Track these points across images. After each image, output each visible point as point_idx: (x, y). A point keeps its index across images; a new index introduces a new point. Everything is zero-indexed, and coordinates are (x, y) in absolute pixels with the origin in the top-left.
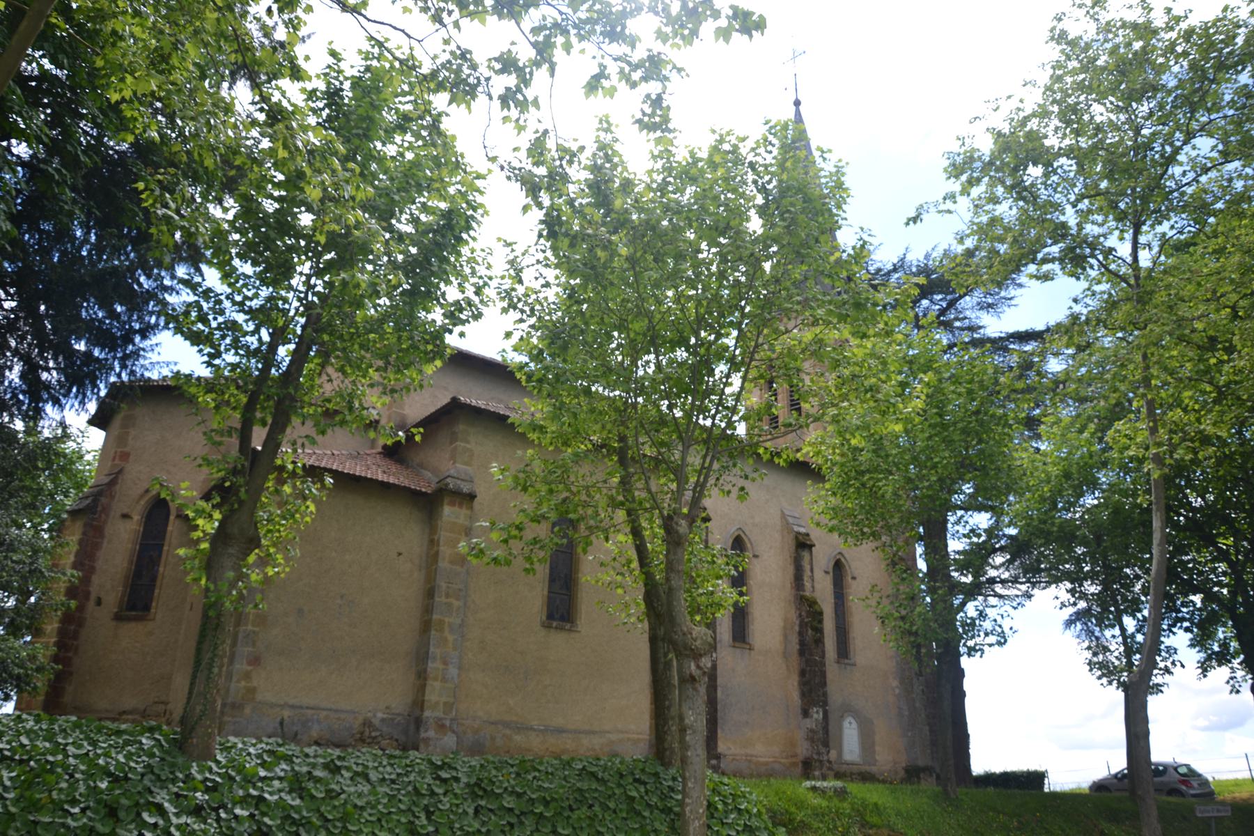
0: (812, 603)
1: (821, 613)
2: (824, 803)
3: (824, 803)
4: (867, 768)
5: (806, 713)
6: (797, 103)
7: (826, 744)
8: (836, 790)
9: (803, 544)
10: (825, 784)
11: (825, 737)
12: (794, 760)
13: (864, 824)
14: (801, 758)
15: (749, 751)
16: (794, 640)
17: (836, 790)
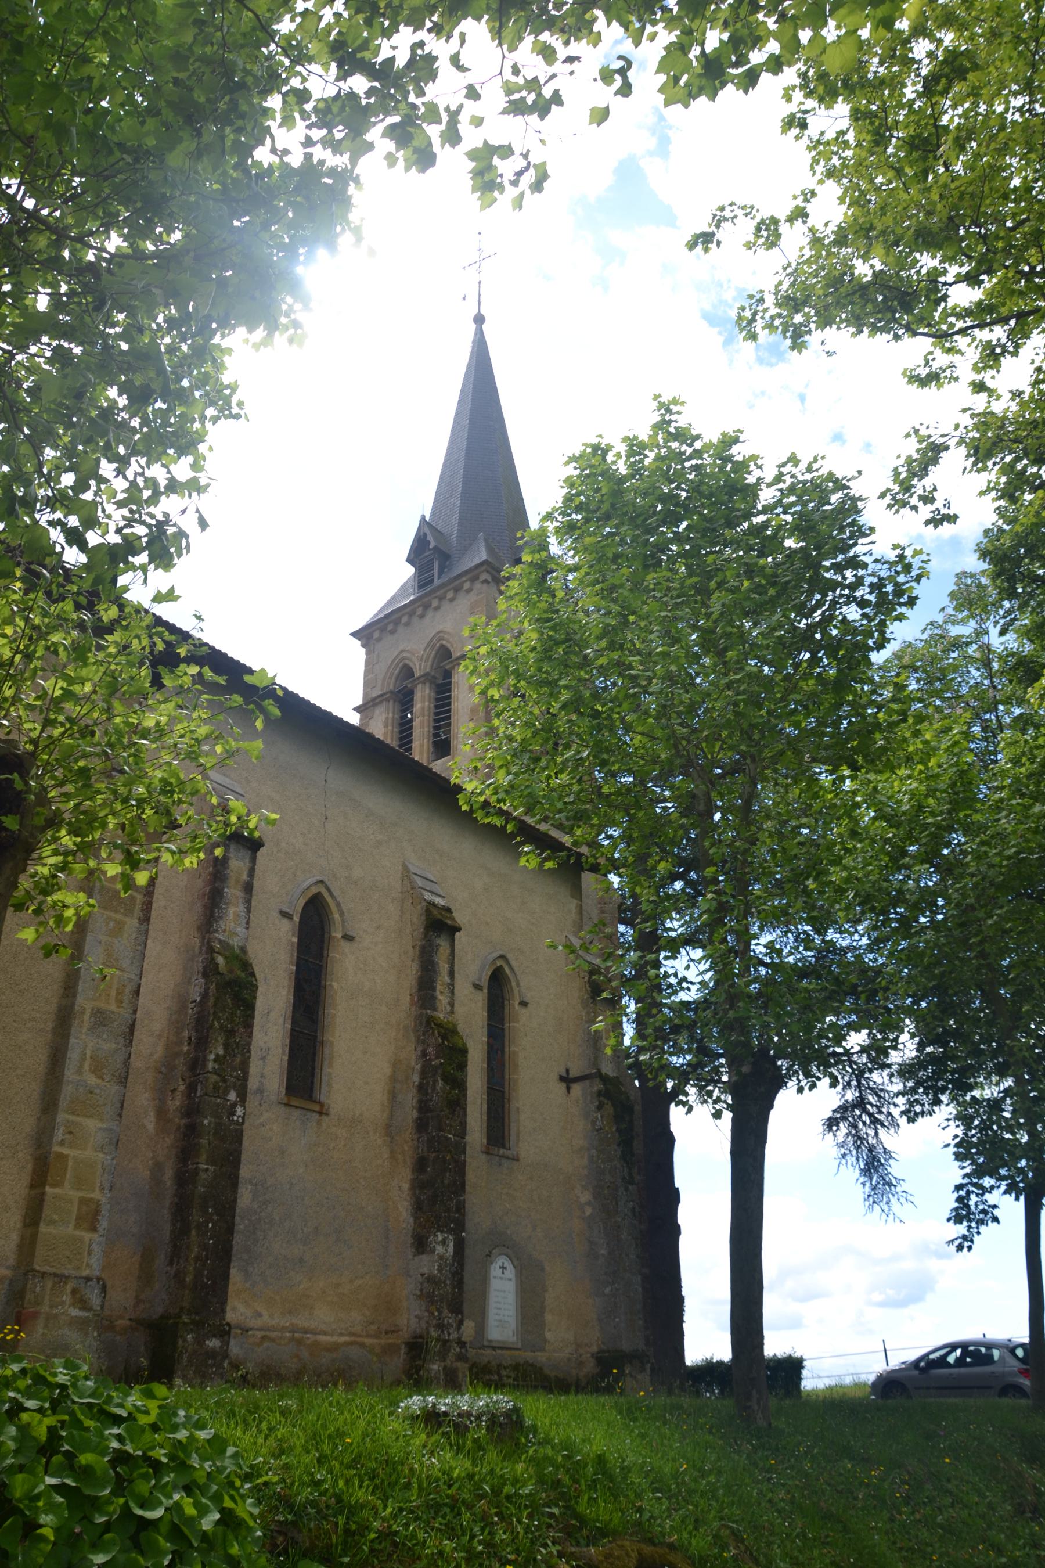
0: (448, 1032)
1: (464, 1052)
2: (460, 1467)
3: (460, 1467)
4: (528, 1355)
5: (421, 1245)
6: (479, 319)
7: (457, 1308)
8: (493, 1420)
9: (439, 925)
10: (464, 1401)
11: (454, 1294)
12: (392, 1339)
13: (575, 1528)
14: (405, 1335)
15: (301, 1322)
16: (409, 1100)
17: (493, 1420)
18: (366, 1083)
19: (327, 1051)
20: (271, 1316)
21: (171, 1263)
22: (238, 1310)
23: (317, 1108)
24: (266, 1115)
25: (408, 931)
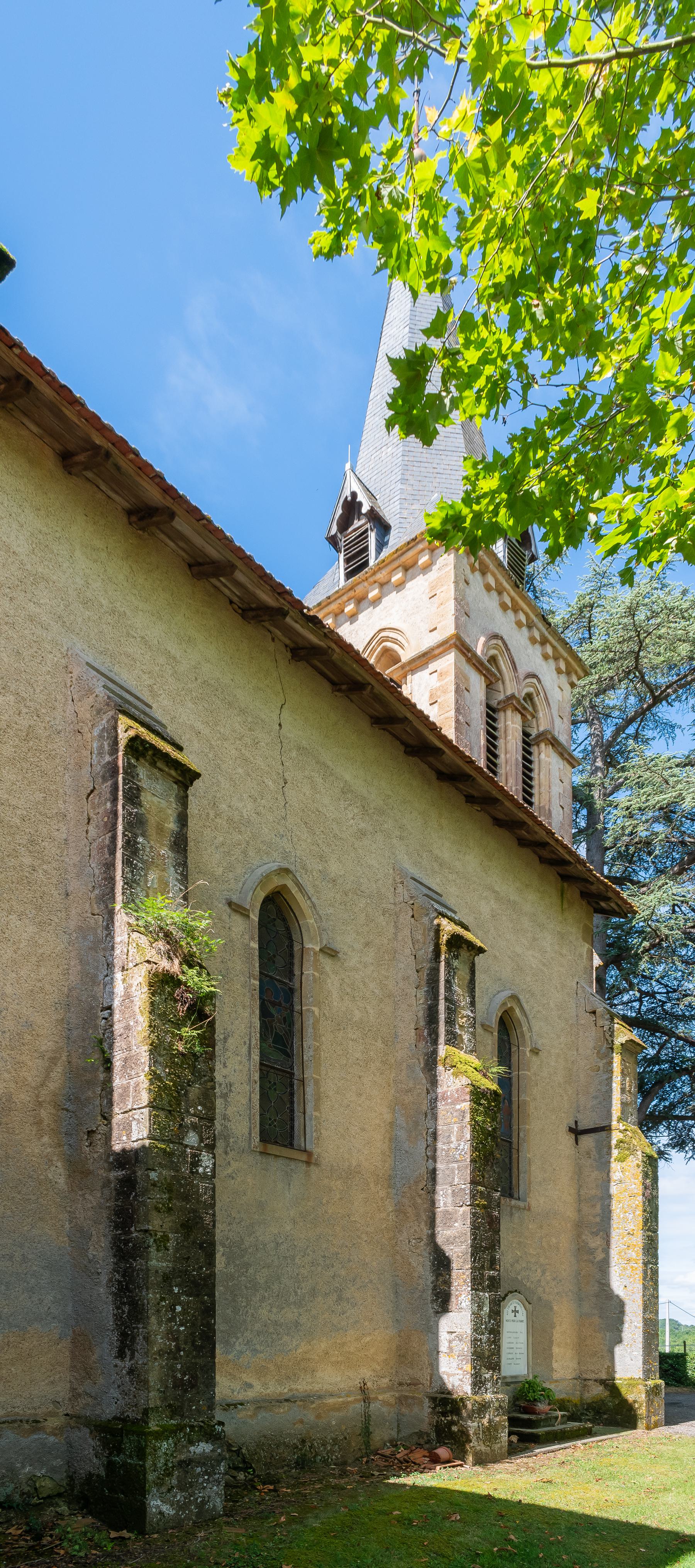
18: (363, 1129)
19: (310, 1090)
20: (265, 1385)
21: (121, 1355)
22: (225, 1386)
23: (304, 1157)
24: (235, 1165)
25: (408, 952)
